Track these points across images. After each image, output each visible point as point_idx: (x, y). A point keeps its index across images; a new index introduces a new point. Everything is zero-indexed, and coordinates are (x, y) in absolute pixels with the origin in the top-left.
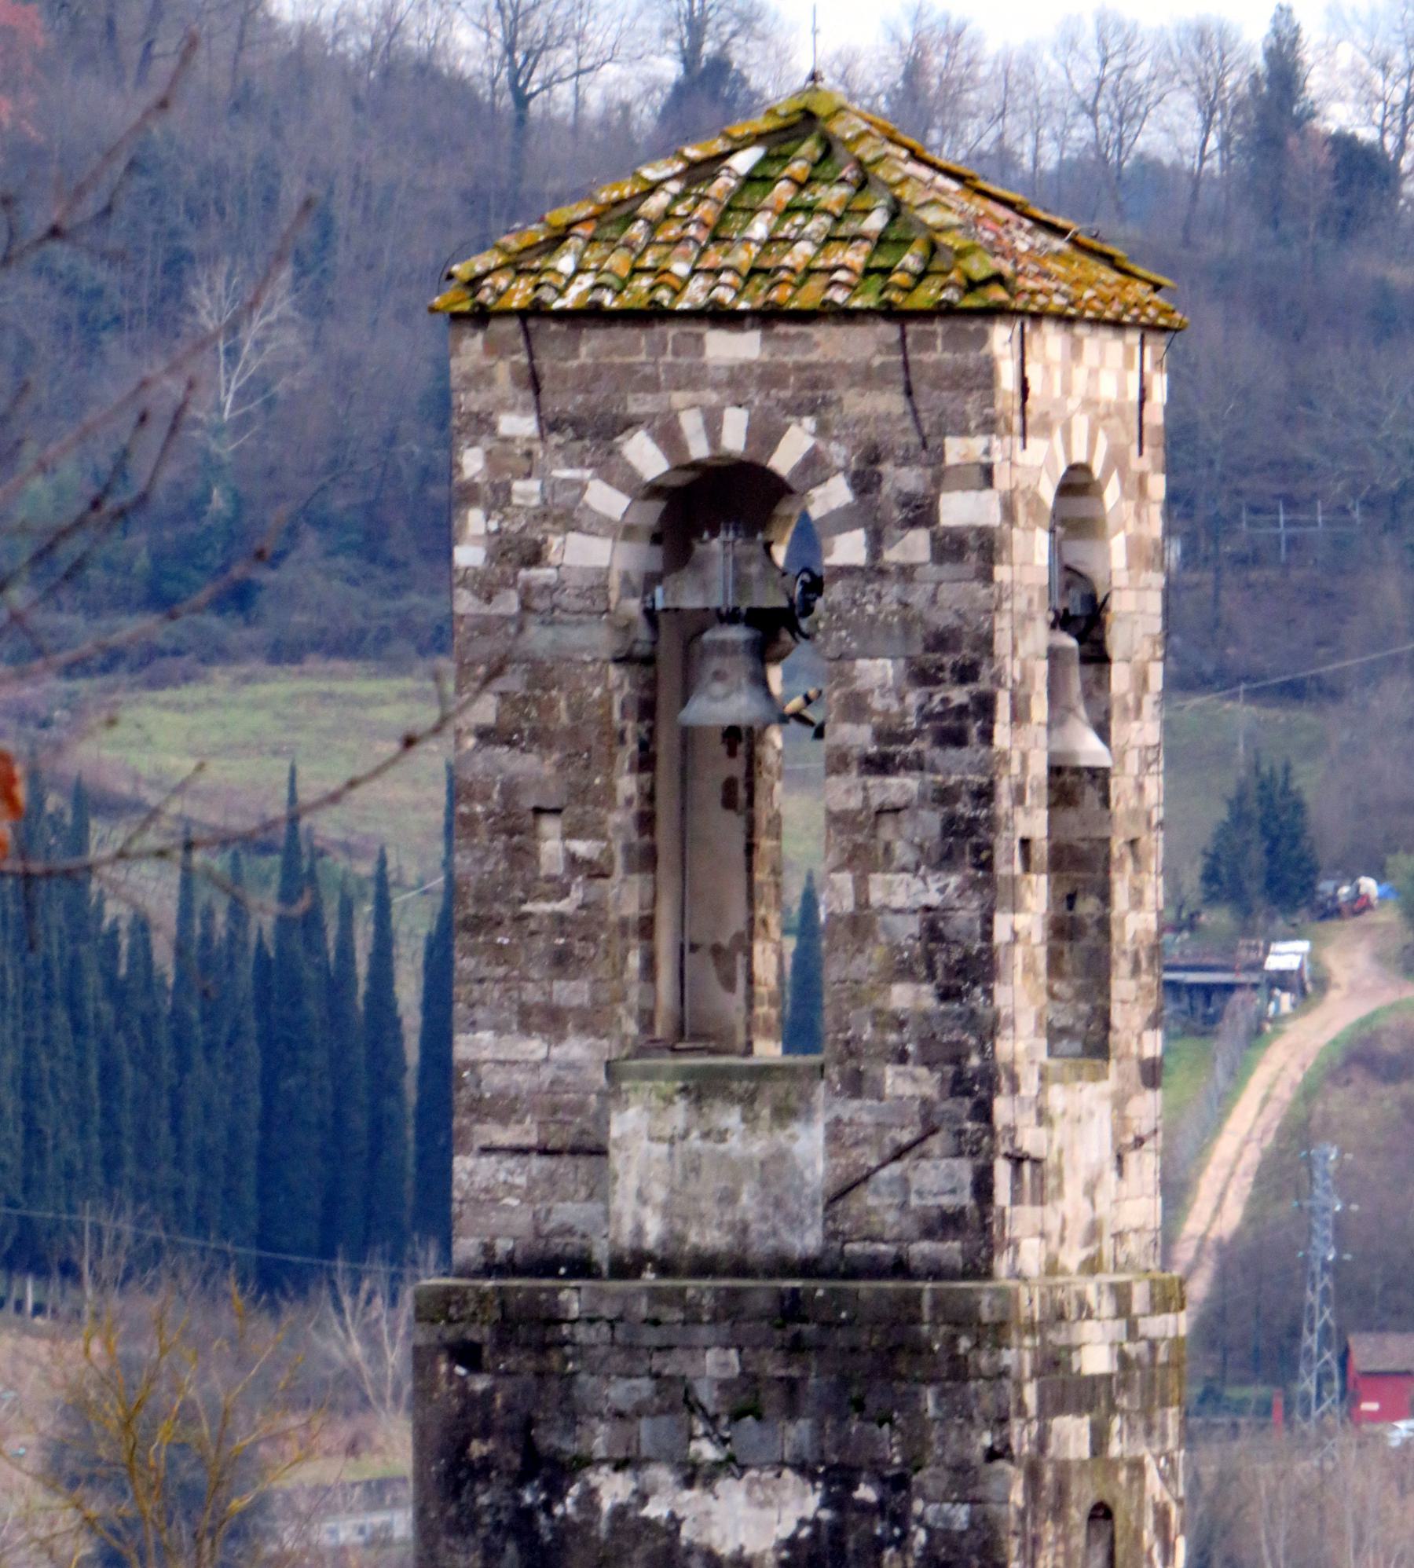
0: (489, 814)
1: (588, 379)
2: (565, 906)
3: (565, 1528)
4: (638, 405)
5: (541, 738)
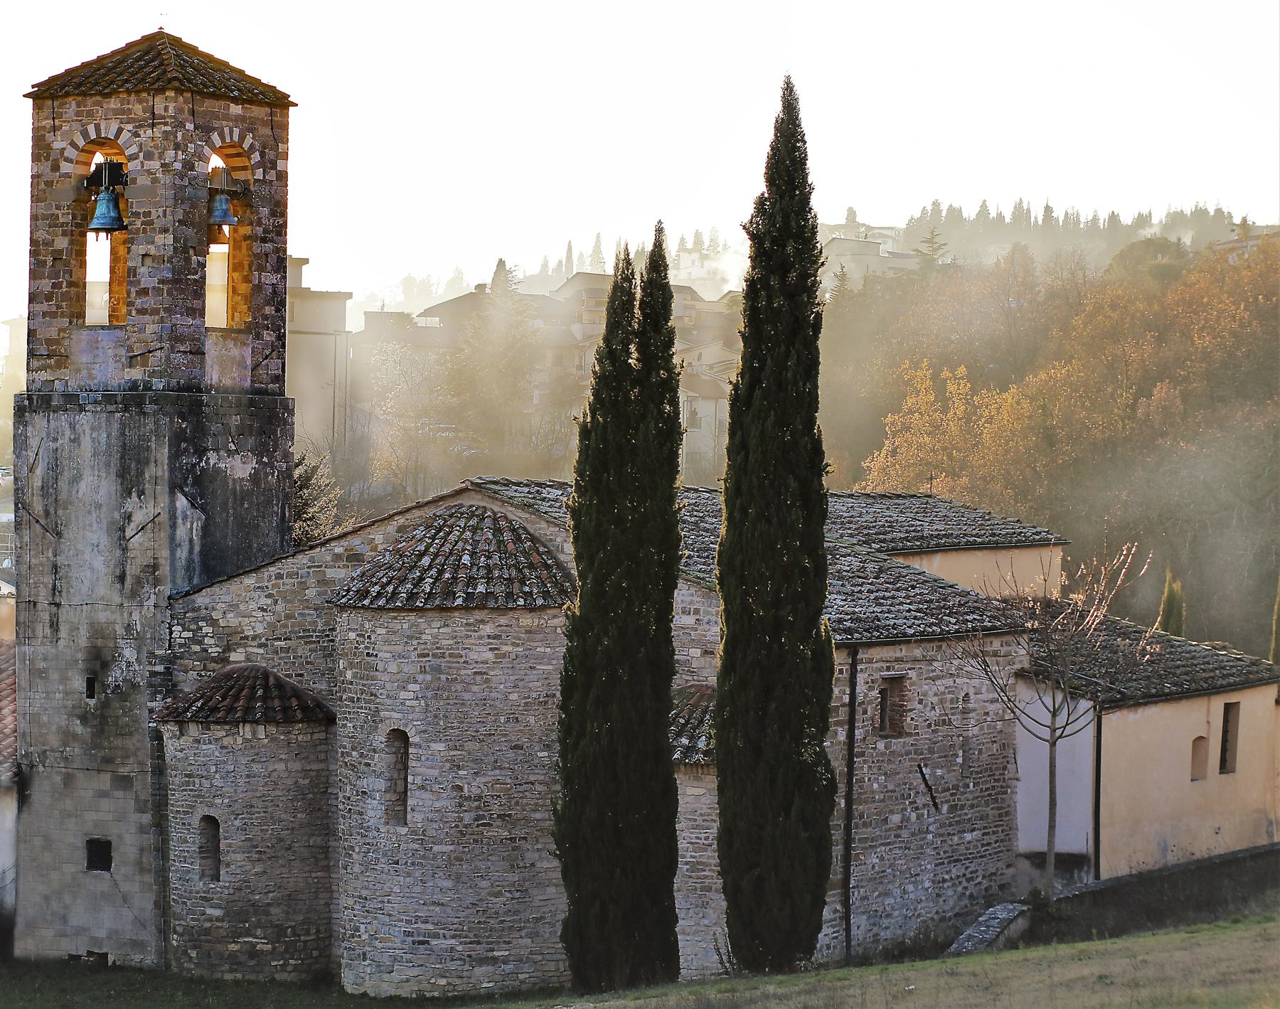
0: (181, 247)
1: (205, 113)
2: (196, 277)
3: (202, 470)
4: (216, 124)
5: (193, 225)
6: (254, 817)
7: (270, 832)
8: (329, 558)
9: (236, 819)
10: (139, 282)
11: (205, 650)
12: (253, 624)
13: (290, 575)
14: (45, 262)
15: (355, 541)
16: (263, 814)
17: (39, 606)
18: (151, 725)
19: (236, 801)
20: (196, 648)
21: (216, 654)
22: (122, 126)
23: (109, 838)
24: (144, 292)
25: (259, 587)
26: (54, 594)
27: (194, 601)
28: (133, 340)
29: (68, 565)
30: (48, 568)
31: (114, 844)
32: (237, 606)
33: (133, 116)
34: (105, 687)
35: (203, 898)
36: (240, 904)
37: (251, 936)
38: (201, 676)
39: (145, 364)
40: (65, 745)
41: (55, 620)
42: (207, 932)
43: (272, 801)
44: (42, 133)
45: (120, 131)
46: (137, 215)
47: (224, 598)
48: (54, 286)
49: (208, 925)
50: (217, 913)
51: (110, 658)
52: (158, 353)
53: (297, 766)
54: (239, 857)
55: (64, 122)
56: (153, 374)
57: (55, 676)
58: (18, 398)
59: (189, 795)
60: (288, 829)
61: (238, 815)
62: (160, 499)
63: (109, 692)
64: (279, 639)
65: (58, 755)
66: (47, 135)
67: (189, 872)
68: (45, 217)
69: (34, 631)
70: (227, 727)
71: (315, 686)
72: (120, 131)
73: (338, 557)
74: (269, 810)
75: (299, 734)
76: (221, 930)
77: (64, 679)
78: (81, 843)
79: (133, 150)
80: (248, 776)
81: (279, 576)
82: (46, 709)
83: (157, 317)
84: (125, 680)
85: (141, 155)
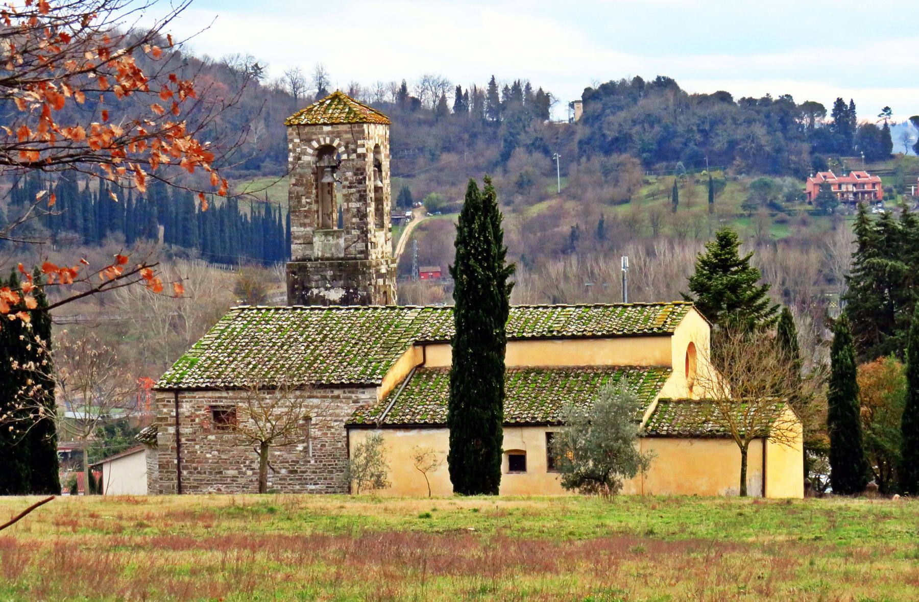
1: (306, 134)
2: (306, 209)
4: (314, 137)
5: (302, 185)
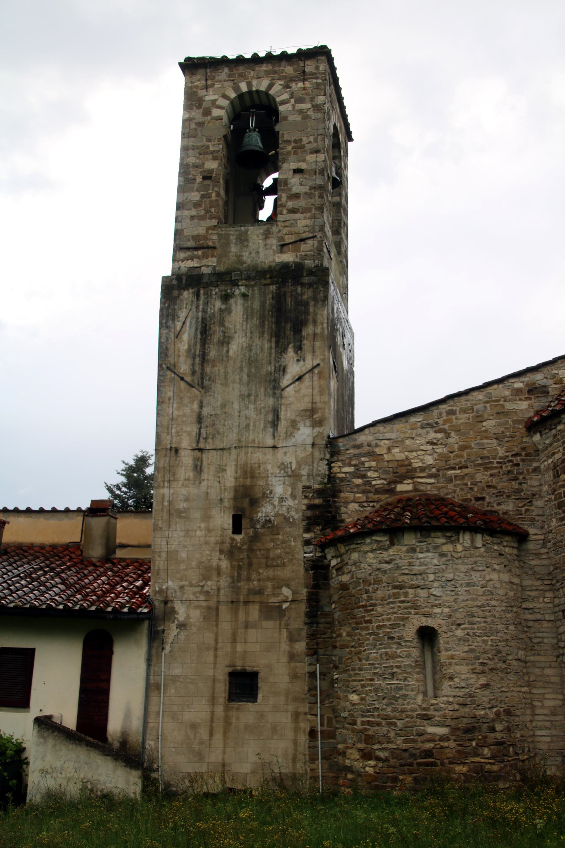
6: (475, 626)
7: (490, 643)
8: (507, 393)
9: (457, 629)
10: (290, 189)
11: (369, 483)
12: (421, 457)
13: (464, 411)
14: (195, 180)
15: (538, 377)
16: (483, 625)
17: (182, 453)
18: (306, 555)
19: (457, 610)
20: (359, 481)
21: (381, 486)
22: (274, 81)
23: (256, 669)
24: (297, 196)
25: (428, 424)
26: (198, 442)
27: (355, 440)
28: (284, 232)
29: (215, 415)
30: (194, 418)
31: (261, 675)
32: (402, 441)
33: (284, 74)
34: (253, 522)
35: (420, 716)
36: (465, 720)
37: (477, 755)
38: (364, 506)
39: (297, 250)
40: (206, 578)
41: (199, 463)
42: (428, 753)
43: (490, 611)
44: (195, 90)
45: (271, 86)
46: (289, 142)
47: (388, 436)
48: (203, 196)
49: (430, 745)
50: (443, 731)
51: (260, 495)
52: (310, 242)
53: (506, 577)
54: (463, 669)
55: (216, 82)
56: (305, 257)
57: (197, 515)
58: (165, 279)
59: (399, 607)
60: (503, 641)
61: (459, 625)
62: (318, 352)
63: (258, 526)
64: (454, 469)
65: (198, 589)
66: (199, 91)
67: (400, 689)
68: (194, 148)
69: (174, 474)
70: (448, 534)
71: (499, 507)
72: (271, 86)
73: (518, 391)
74: (489, 620)
75: (507, 546)
76: (447, 751)
77: (207, 517)
78: (222, 675)
79: (285, 96)
80: (468, 585)
81: (451, 413)
82: (185, 547)
83: (308, 215)
84: (277, 515)
85: (293, 101)
